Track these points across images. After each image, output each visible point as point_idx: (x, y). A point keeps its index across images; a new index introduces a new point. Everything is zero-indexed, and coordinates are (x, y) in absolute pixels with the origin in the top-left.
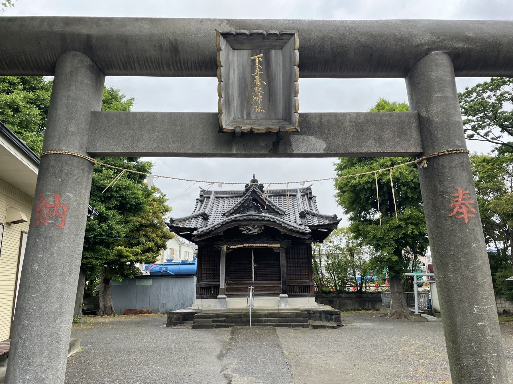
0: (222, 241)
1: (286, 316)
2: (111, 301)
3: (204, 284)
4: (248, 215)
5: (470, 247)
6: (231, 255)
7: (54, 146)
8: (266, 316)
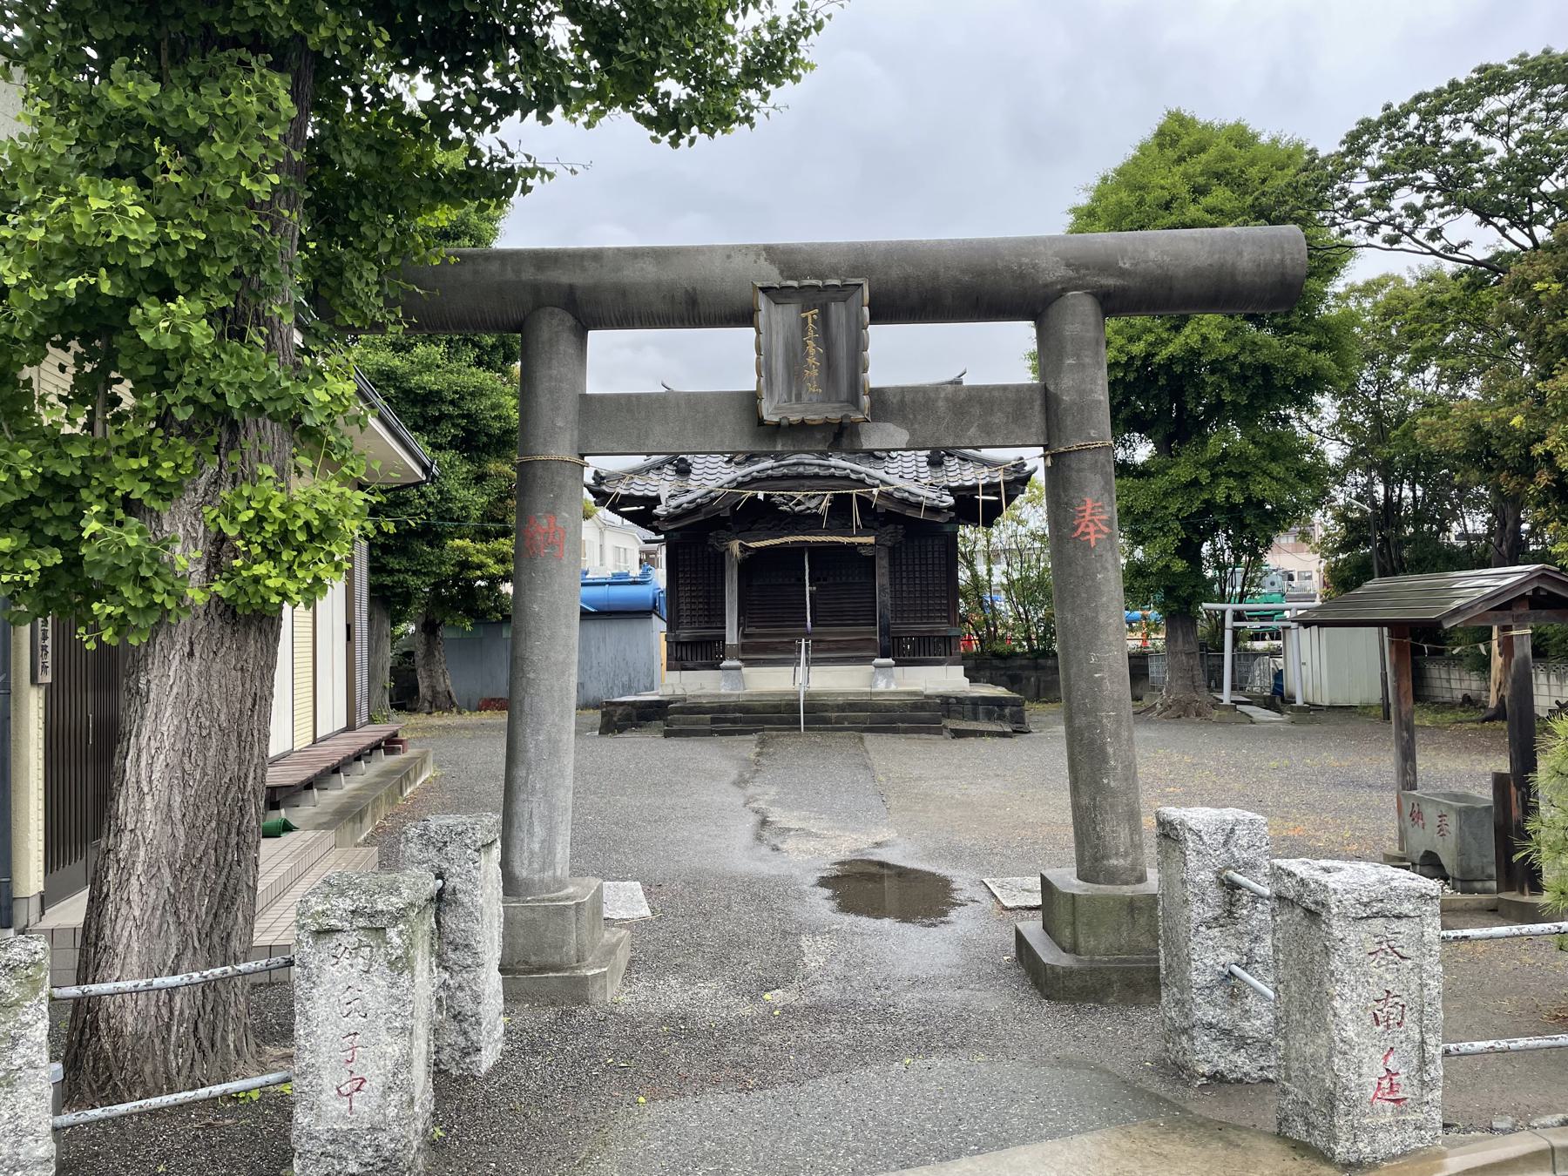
0: (728, 529)
1: (888, 708)
2: (447, 676)
3: (684, 634)
4: (794, 464)
5: (1094, 580)
6: (752, 565)
7: (540, 449)
8: (841, 708)
